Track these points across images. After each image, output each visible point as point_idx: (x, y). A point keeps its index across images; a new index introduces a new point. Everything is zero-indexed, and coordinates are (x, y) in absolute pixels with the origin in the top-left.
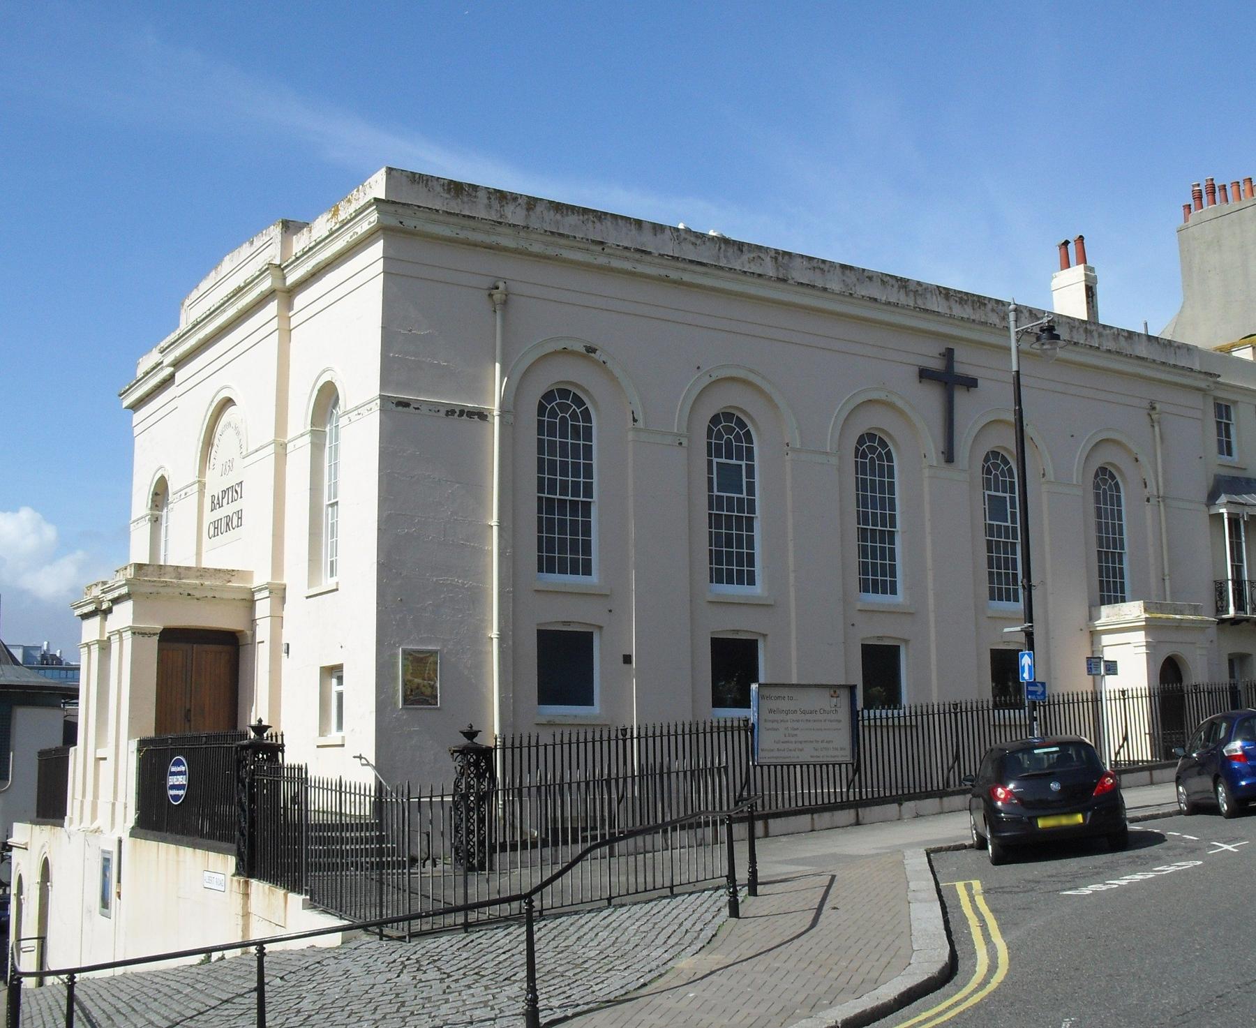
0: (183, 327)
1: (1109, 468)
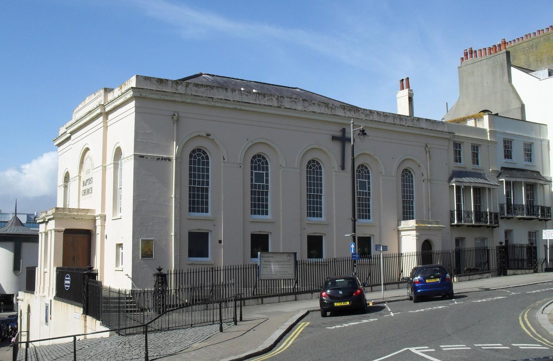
0: (74, 120)
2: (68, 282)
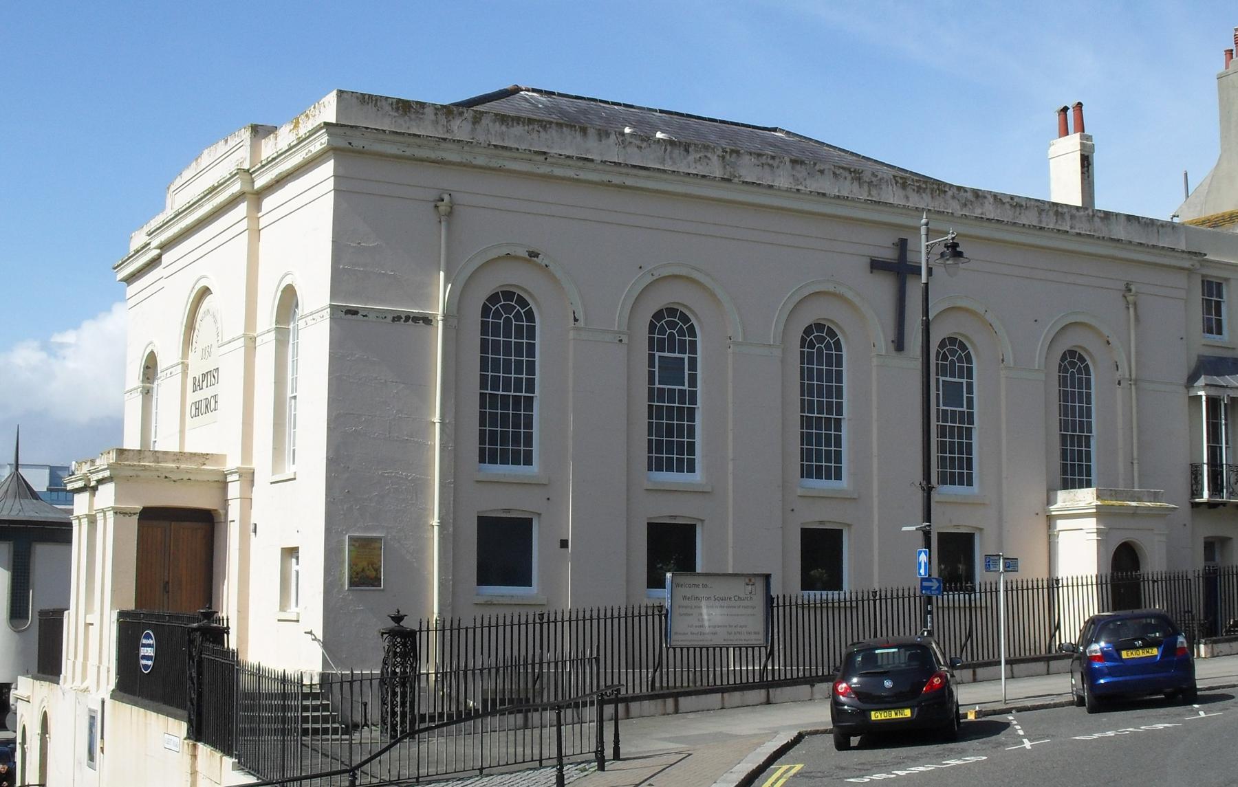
0: (169, 213)
2: (150, 652)
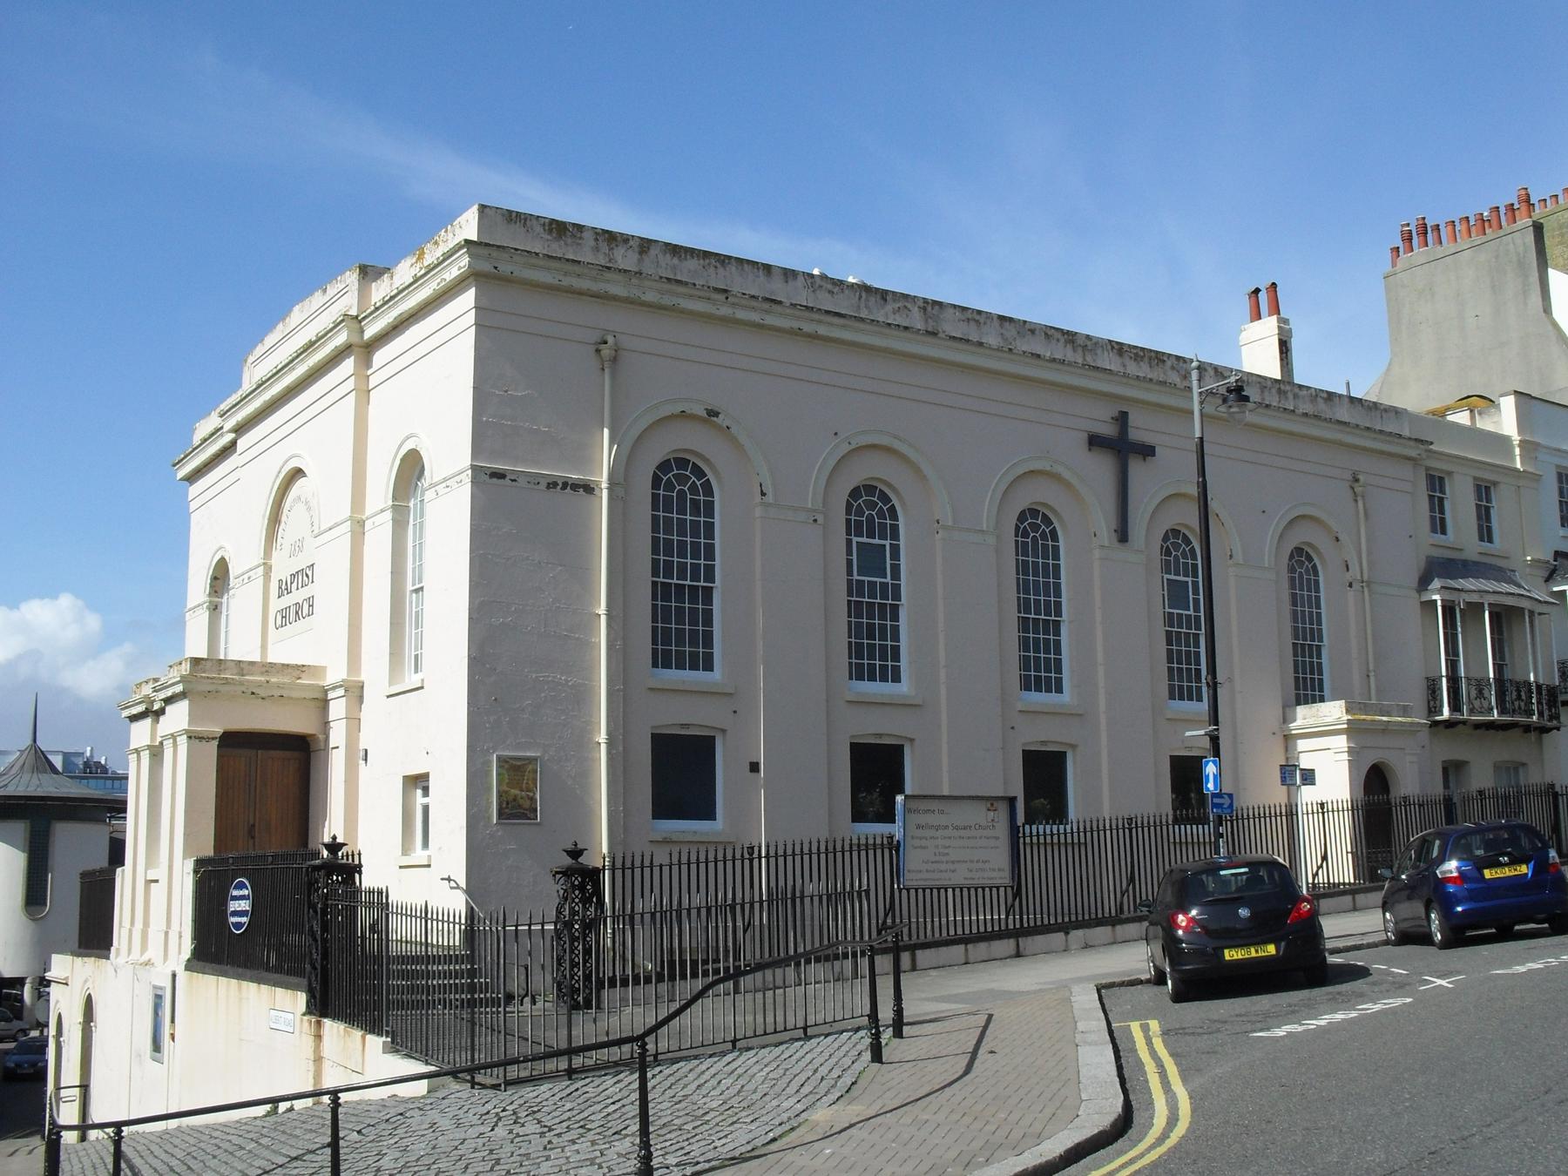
0: (247, 386)
1: (1306, 548)
2: (244, 905)
